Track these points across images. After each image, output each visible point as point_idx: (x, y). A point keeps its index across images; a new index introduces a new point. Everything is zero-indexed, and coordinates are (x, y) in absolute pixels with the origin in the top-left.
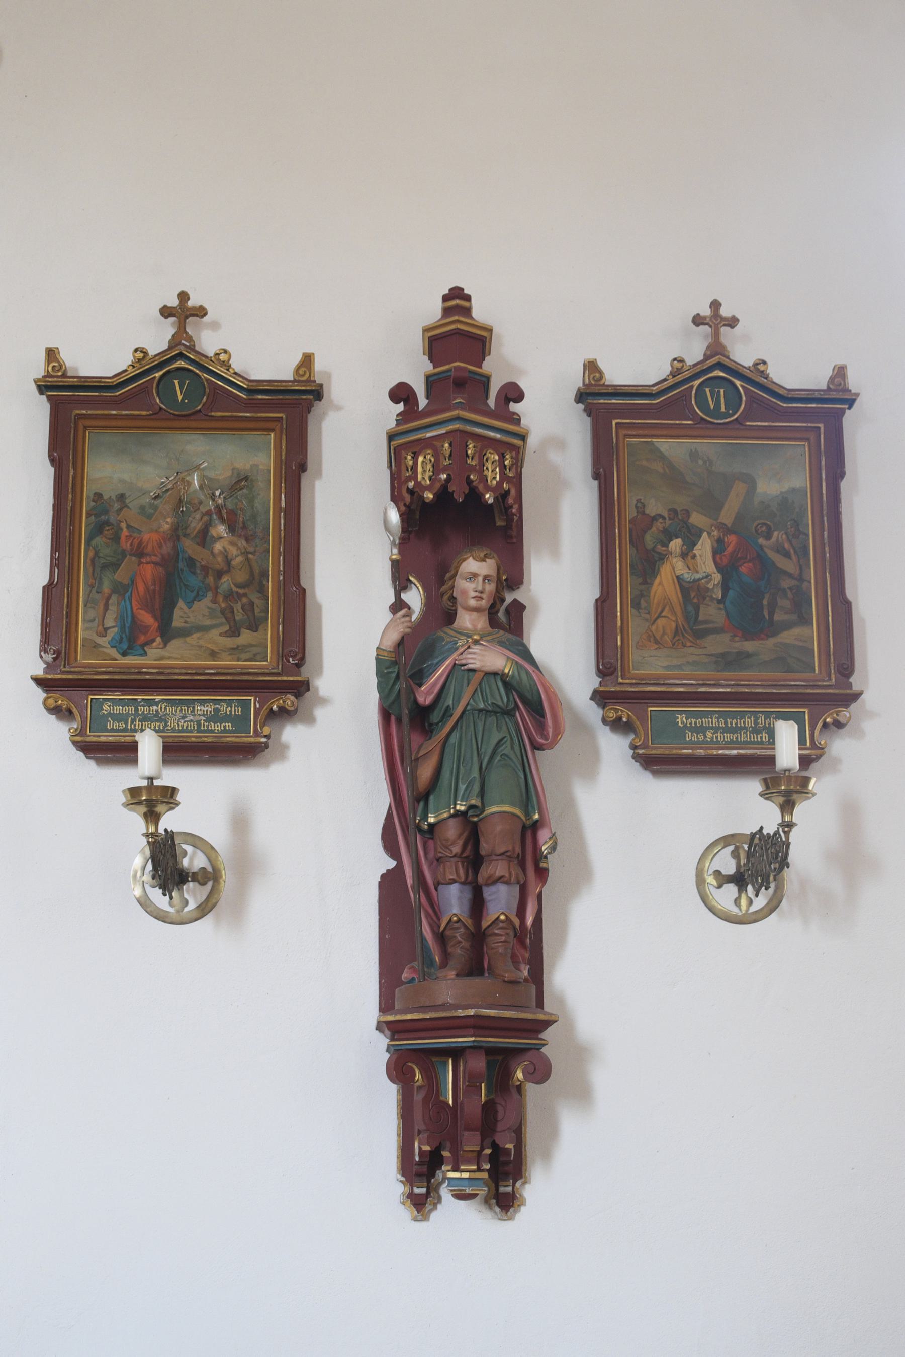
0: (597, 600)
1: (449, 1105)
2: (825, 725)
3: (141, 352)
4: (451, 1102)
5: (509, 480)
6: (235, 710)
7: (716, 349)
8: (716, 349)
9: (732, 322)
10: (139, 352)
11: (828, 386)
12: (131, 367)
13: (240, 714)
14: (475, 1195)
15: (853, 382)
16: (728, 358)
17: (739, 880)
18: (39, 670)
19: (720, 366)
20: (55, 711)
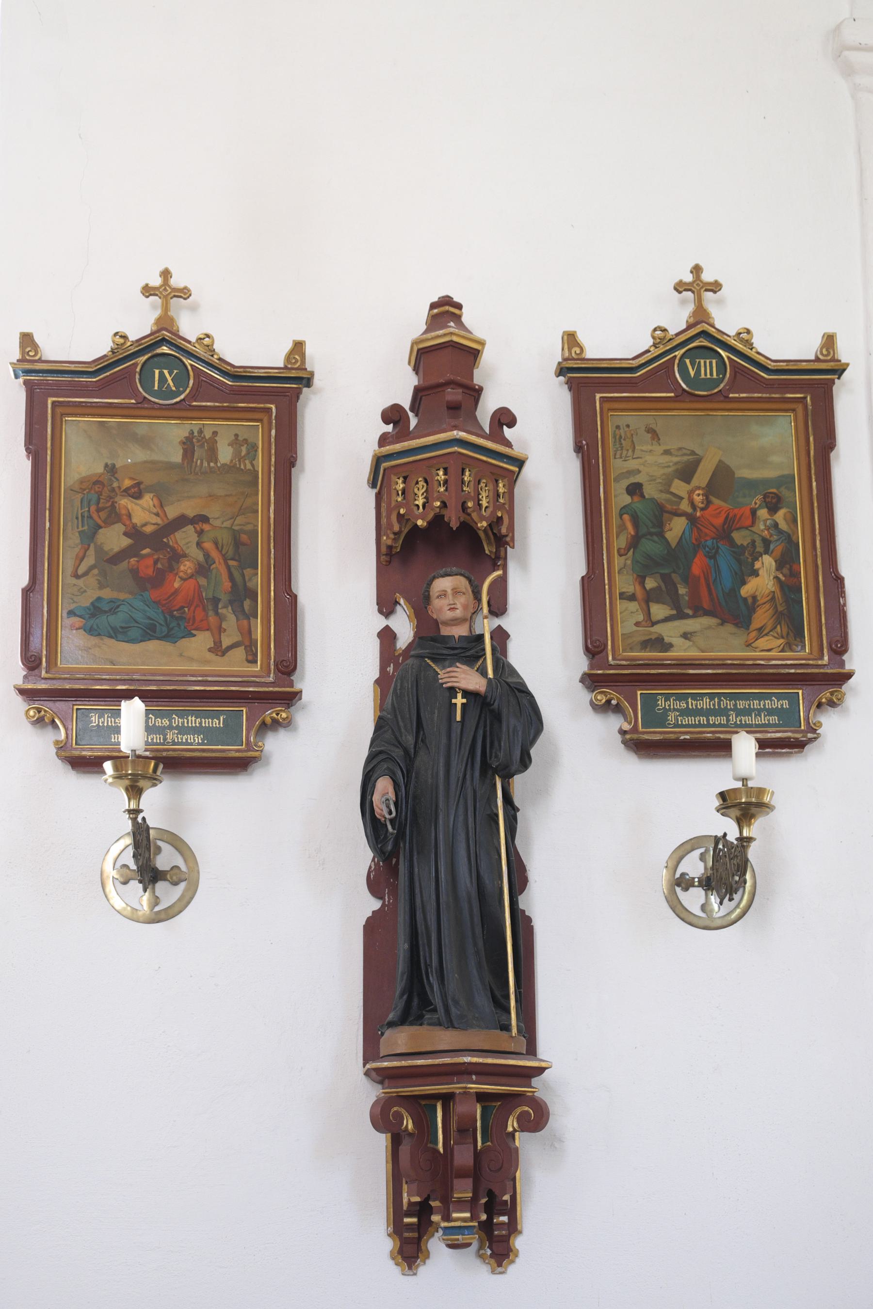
0: (583, 578)
1: (439, 1152)
2: (264, 724)
3: (121, 337)
4: (441, 1150)
5: (501, 507)
6: (108, 721)
7: (700, 315)
8: (700, 315)
9: (715, 287)
10: (118, 337)
11: (817, 357)
12: (110, 353)
13: (222, 726)
14: (468, 1245)
15: (844, 352)
16: (713, 326)
17: (707, 883)
18: (19, 681)
19: (704, 334)
20: (39, 722)
